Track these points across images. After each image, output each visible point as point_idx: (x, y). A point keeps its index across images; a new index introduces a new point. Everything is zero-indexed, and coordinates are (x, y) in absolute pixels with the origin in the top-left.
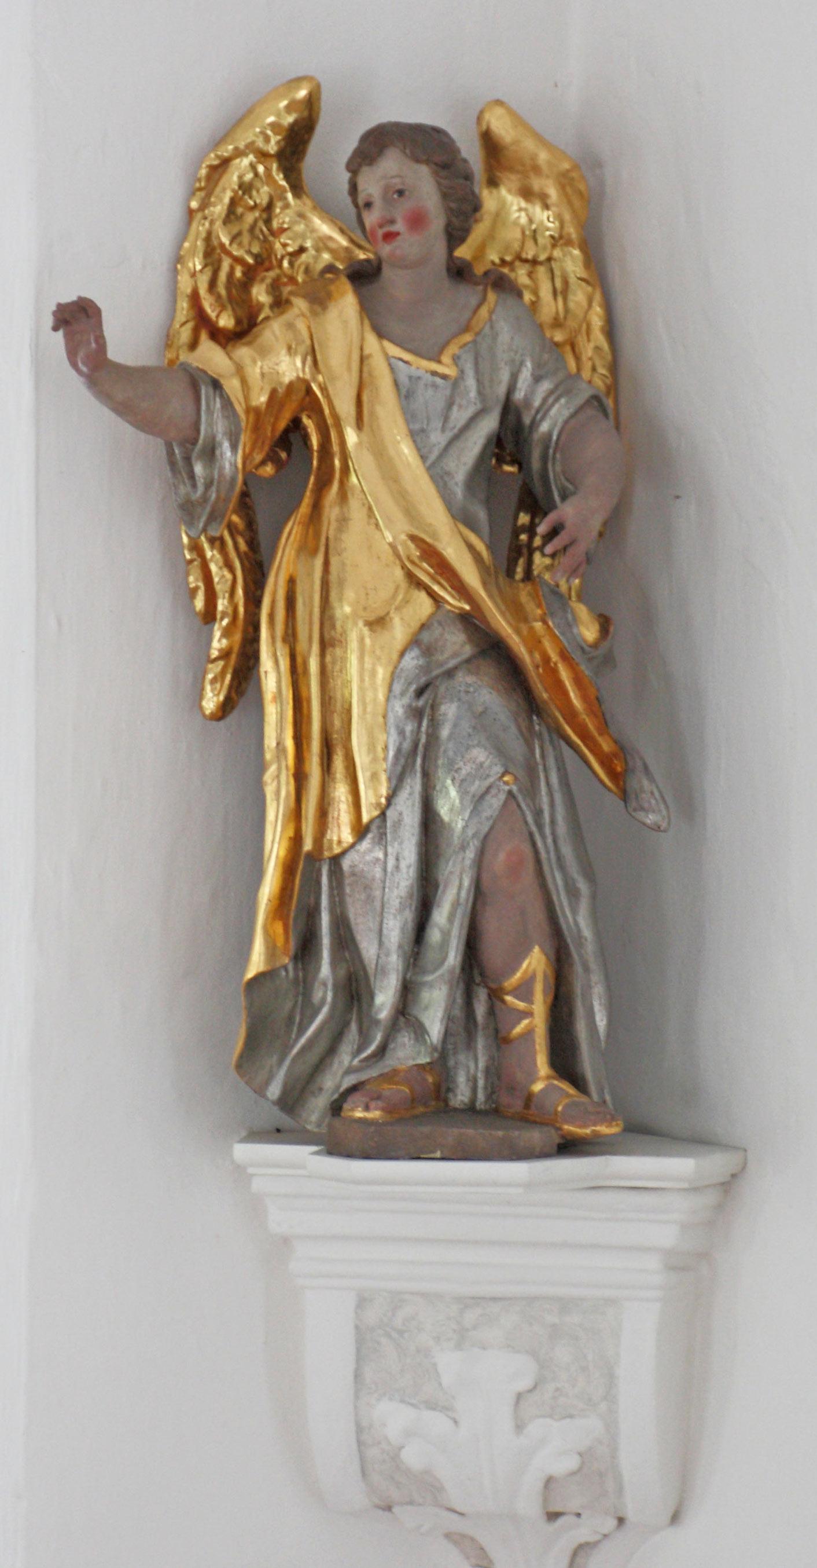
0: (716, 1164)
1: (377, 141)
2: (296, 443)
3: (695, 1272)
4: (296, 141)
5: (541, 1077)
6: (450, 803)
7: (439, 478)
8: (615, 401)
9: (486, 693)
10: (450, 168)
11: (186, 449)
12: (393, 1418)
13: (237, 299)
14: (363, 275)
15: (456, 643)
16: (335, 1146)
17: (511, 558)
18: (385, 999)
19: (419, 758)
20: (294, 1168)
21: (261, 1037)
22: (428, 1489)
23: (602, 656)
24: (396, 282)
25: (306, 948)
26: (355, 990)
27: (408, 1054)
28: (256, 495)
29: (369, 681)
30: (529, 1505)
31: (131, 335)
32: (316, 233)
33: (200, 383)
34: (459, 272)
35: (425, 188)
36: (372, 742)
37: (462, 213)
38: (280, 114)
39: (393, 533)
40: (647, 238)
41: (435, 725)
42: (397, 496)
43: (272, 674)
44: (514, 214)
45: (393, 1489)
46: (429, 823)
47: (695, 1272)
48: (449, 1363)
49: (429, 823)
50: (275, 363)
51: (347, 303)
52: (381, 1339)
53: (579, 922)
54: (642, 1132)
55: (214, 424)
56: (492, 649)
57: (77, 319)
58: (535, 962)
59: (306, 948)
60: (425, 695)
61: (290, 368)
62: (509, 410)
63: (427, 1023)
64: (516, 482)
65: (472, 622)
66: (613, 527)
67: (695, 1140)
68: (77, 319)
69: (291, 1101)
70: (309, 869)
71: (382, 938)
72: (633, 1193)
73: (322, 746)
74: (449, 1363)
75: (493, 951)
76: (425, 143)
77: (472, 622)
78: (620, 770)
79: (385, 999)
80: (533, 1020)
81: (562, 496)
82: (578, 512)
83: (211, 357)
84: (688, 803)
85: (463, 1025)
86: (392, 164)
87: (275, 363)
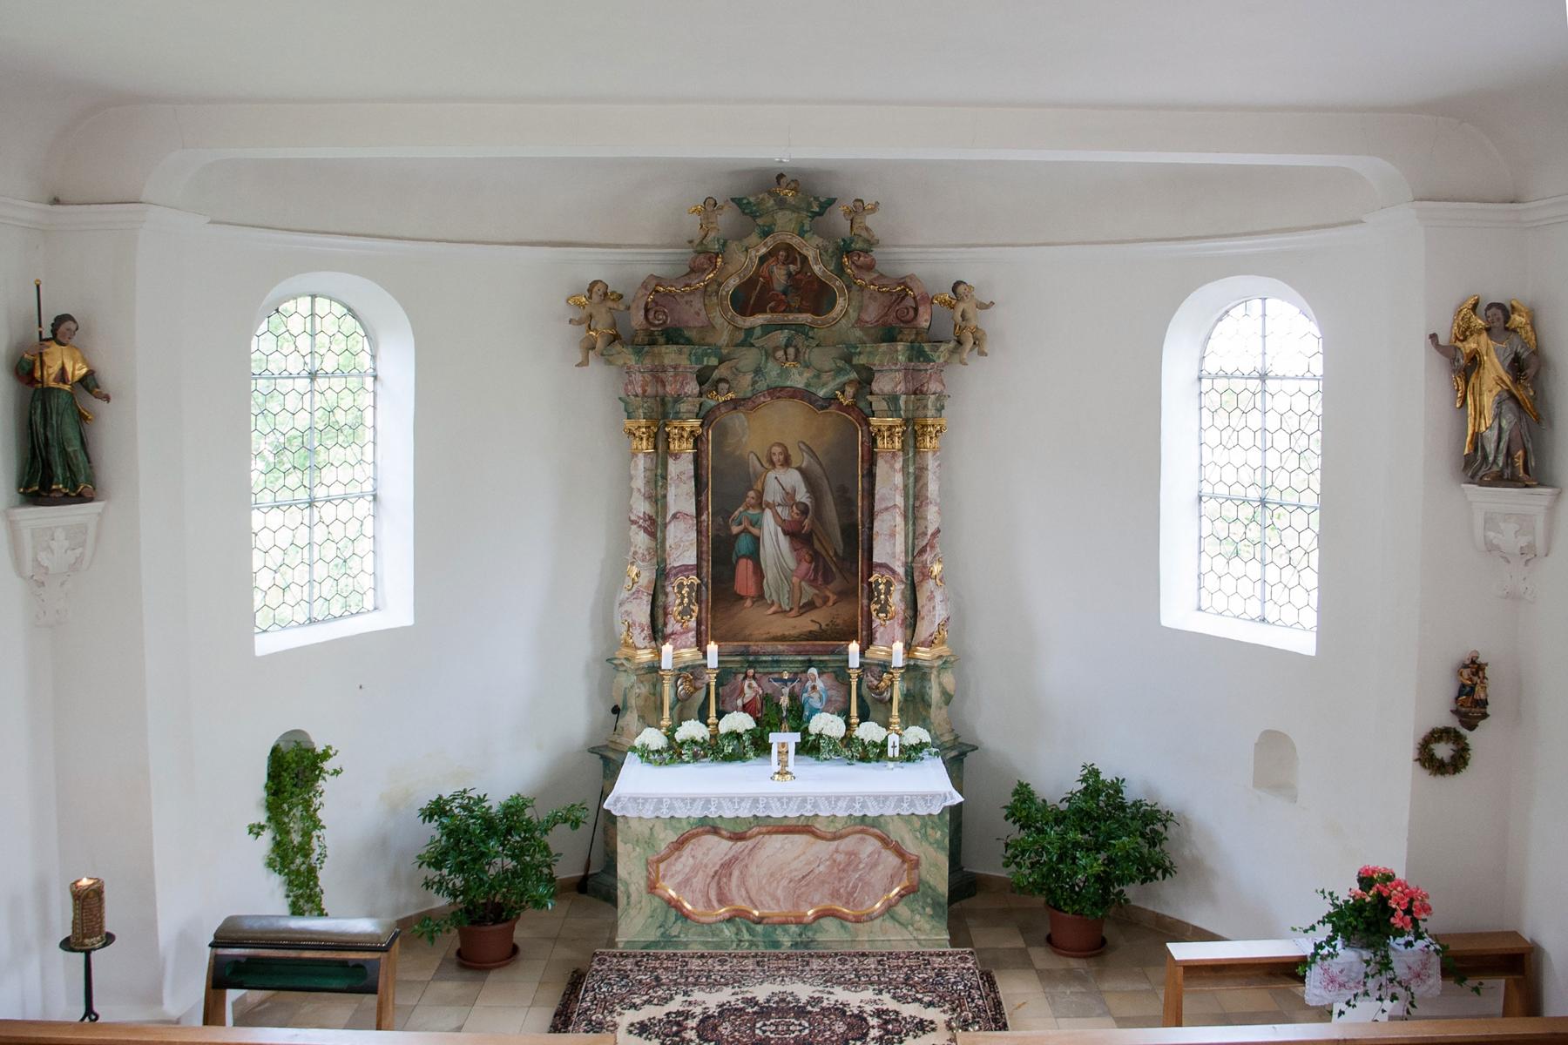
0: (1556, 491)
1: (1491, 306)
2: (1474, 361)
3: (1551, 511)
4: (1475, 307)
5: (1521, 473)
6: (1504, 423)
7: (1502, 363)
8: (1537, 352)
9: (1511, 404)
10: (1505, 311)
11: (1454, 360)
12: (1491, 534)
13: (1465, 333)
14: (1488, 330)
15: (1505, 395)
16: (1481, 485)
17: (1516, 380)
18: (1491, 459)
19: (1498, 416)
20: (1474, 490)
21: (1466, 467)
22: (1498, 548)
23: (1534, 399)
24: (1494, 331)
25: (1476, 450)
26: (1485, 457)
27: (1495, 469)
28: (1468, 369)
29: (1488, 401)
30: (1517, 551)
31: (1443, 340)
32: (1479, 322)
33: (1457, 349)
34: (1507, 329)
35: (1500, 313)
36: (1489, 413)
37: (1507, 318)
38: (1472, 301)
39: (1493, 375)
40: (1544, 323)
41: (1031, 892)
42: (1494, 370)
43: (1469, 400)
44: (1517, 319)
45: (1491, 548)
46: (1500, 427)
47: (1551, 511)
48: (1502, 525)
49: (1500, 427)
50: (1471, 345)
51: (1485, 334)
52: (1489, 521)
53: (1529, 446)
54: (1541, 485)
55: (1459, 356)
56: (1512, 397)
57: (1433, 337)
58: (1520, 453)
59: (1476, 450)
60: (1499, 404)
61: (1474, 346)
62: (1516, 354)
63: (784, 542)
64: (1517, 367)
65: (1509, 391)
66: (1537, 373)
67: (1552, 486)
68: (1433, 337)
69: (1473, 477)
70: (1477, 436)
71: (1491, 448)
72: (568, 239)
73: (1479, 413)
74: (1502, 525)
75: (1513, 448)
76: (1500, 306)
77: (1509, 391)
78: (1538, 419)
79: (1491, 459)
80: (1520, 463)
81: (1527, 369)
82: (1530, 372)
83: (1459, 344)
84: (1551, 424)
85: (1506, 464)
86: (1493, 310)
87: (1471, 345)
